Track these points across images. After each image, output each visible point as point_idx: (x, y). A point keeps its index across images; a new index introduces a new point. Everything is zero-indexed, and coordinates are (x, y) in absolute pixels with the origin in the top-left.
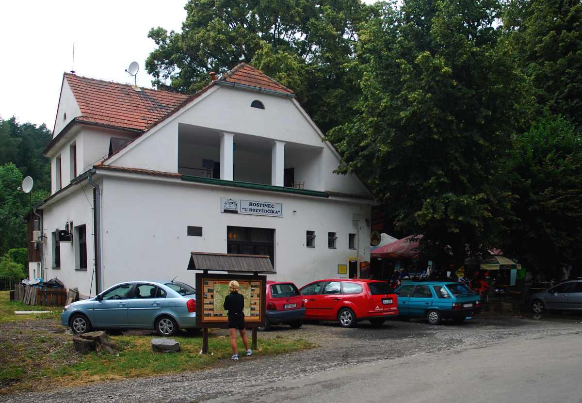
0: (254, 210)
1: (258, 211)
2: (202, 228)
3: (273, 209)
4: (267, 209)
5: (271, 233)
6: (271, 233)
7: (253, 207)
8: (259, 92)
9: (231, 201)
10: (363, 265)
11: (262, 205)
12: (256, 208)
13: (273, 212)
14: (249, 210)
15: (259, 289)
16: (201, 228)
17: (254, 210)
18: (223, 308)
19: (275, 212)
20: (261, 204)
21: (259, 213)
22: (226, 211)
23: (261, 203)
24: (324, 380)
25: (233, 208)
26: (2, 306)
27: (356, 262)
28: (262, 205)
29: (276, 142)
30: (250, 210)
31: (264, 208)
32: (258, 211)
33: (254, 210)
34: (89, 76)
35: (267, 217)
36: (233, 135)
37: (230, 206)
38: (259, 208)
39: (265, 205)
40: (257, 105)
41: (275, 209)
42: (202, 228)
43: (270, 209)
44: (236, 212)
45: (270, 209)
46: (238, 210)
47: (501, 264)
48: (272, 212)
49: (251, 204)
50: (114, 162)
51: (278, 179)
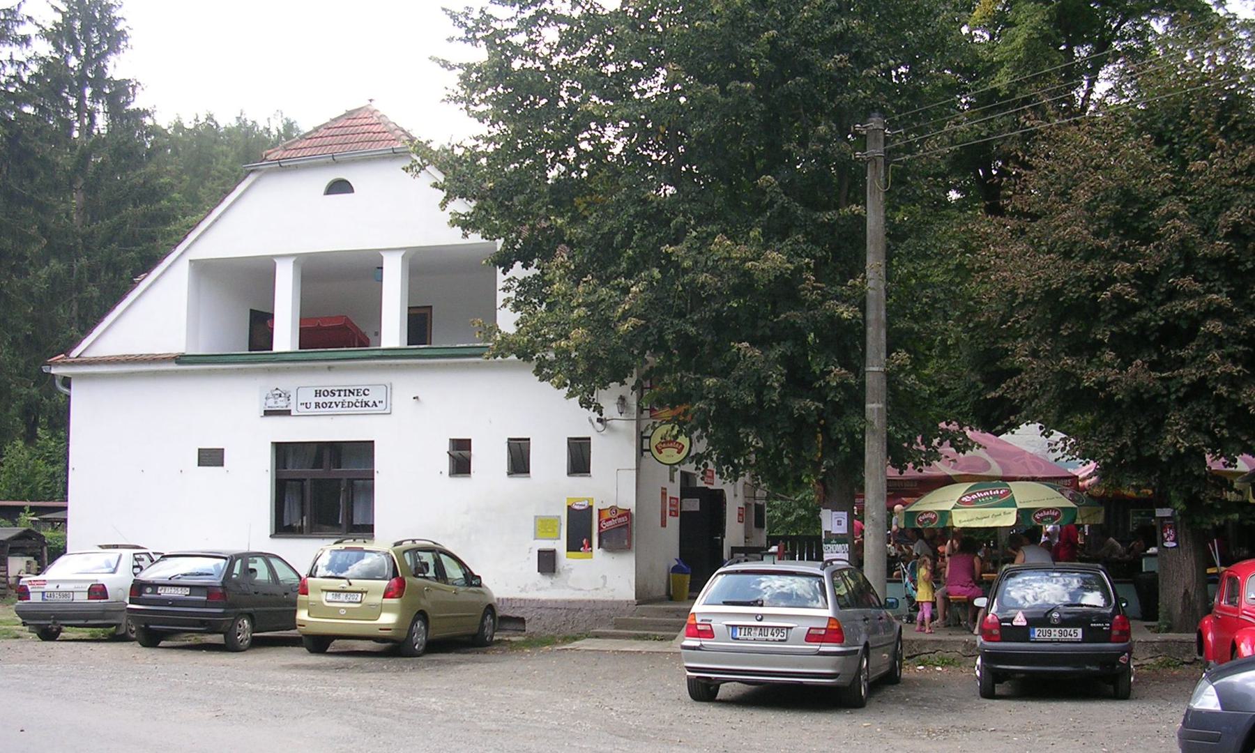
0: (325, 401)
1: (333, 405)
2: (200, 450)
3: (365, 399)
4: (353, 399)
5: (365, 450)
6: (365, 450)
7: (321, 400)
8: (335, 162)
9: (278, 392)
10: (607, 515)
11: (342, 393)
12: (329, 399)
13: (366, 404)
14: (313, 405)
15: (1250, 654)
16: (511, 441)
17: (325, 405)
18: (979, 694)
19: (370, 404)
20: (340, 391)
21: (334, 410)
22: (268, 413)
23: (340, 388)
24: (9, 640)
25: (281, 404)
26: (1, 573)
27: (591, 507)
28: (342, 393)
29: (382, 254)
30: (317, 405)
31: (348, 399)
32: (333, 405)
33: (325, 405)
34: (323, 119)
35: (352, 417)
36: (293, 259)
37: (276, 402)
38: (336, 399)
39: (350, 391)
40: (340, 187)
41: (370, 399)
42: (200, 450)
43: (360, 399)
44: (287, 413)
45: (360, 399)
46: (292, 407)
47: (1020, 506)
48: (360, 402)
49: (318, 393)
50: (85, 350)
51: (393, 332)
